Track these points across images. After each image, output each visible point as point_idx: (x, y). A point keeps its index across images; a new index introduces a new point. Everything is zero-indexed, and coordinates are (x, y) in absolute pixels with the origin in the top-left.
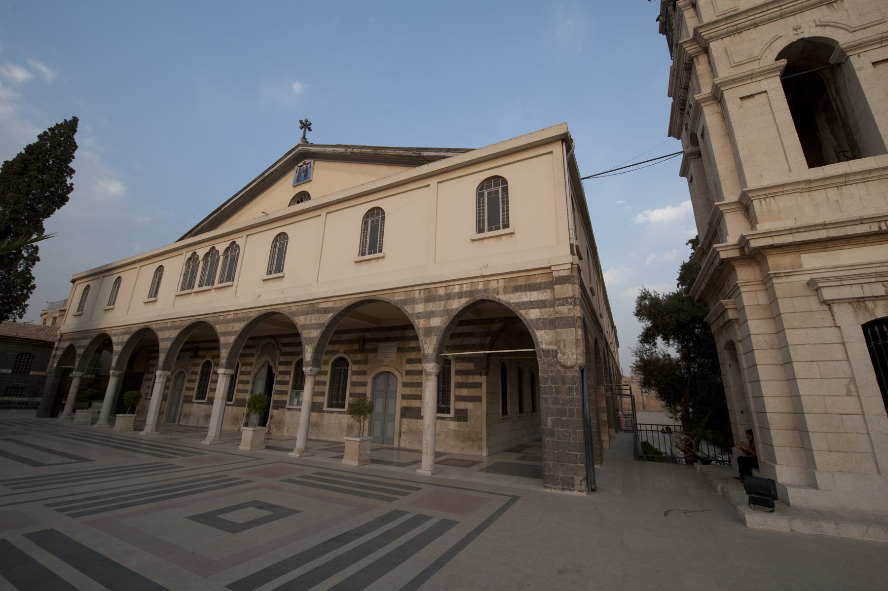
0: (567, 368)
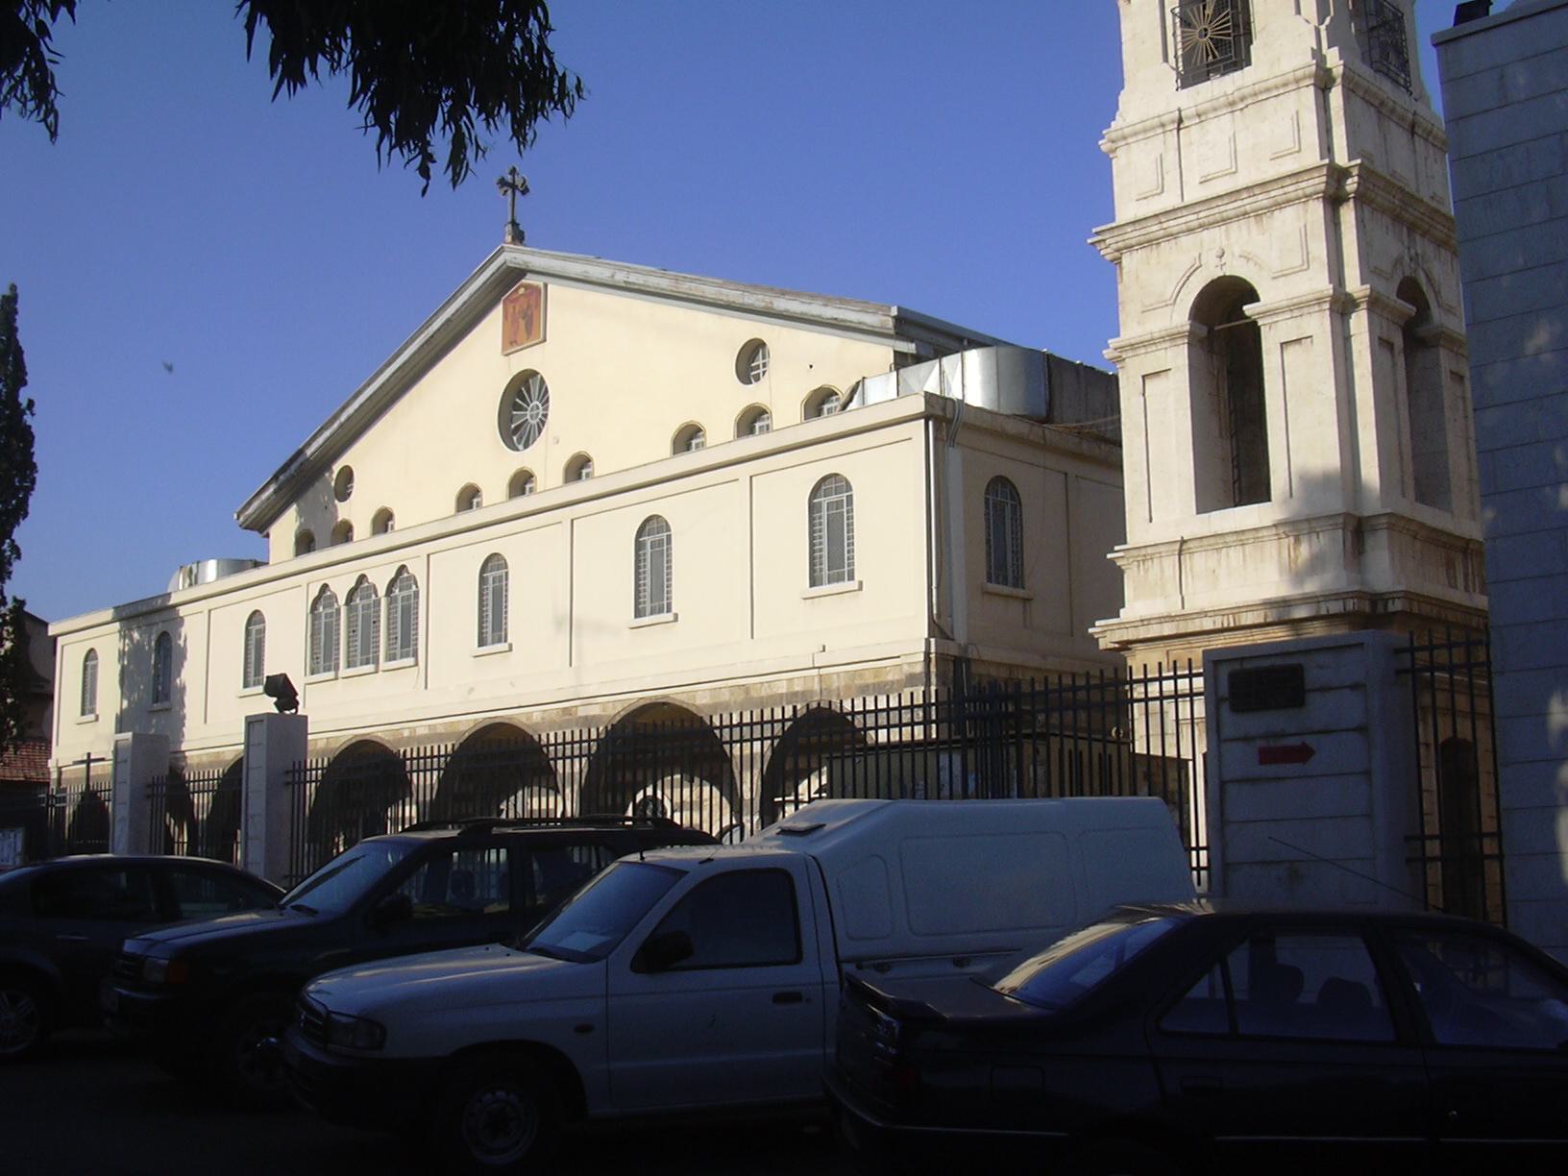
0: (1064, 835)
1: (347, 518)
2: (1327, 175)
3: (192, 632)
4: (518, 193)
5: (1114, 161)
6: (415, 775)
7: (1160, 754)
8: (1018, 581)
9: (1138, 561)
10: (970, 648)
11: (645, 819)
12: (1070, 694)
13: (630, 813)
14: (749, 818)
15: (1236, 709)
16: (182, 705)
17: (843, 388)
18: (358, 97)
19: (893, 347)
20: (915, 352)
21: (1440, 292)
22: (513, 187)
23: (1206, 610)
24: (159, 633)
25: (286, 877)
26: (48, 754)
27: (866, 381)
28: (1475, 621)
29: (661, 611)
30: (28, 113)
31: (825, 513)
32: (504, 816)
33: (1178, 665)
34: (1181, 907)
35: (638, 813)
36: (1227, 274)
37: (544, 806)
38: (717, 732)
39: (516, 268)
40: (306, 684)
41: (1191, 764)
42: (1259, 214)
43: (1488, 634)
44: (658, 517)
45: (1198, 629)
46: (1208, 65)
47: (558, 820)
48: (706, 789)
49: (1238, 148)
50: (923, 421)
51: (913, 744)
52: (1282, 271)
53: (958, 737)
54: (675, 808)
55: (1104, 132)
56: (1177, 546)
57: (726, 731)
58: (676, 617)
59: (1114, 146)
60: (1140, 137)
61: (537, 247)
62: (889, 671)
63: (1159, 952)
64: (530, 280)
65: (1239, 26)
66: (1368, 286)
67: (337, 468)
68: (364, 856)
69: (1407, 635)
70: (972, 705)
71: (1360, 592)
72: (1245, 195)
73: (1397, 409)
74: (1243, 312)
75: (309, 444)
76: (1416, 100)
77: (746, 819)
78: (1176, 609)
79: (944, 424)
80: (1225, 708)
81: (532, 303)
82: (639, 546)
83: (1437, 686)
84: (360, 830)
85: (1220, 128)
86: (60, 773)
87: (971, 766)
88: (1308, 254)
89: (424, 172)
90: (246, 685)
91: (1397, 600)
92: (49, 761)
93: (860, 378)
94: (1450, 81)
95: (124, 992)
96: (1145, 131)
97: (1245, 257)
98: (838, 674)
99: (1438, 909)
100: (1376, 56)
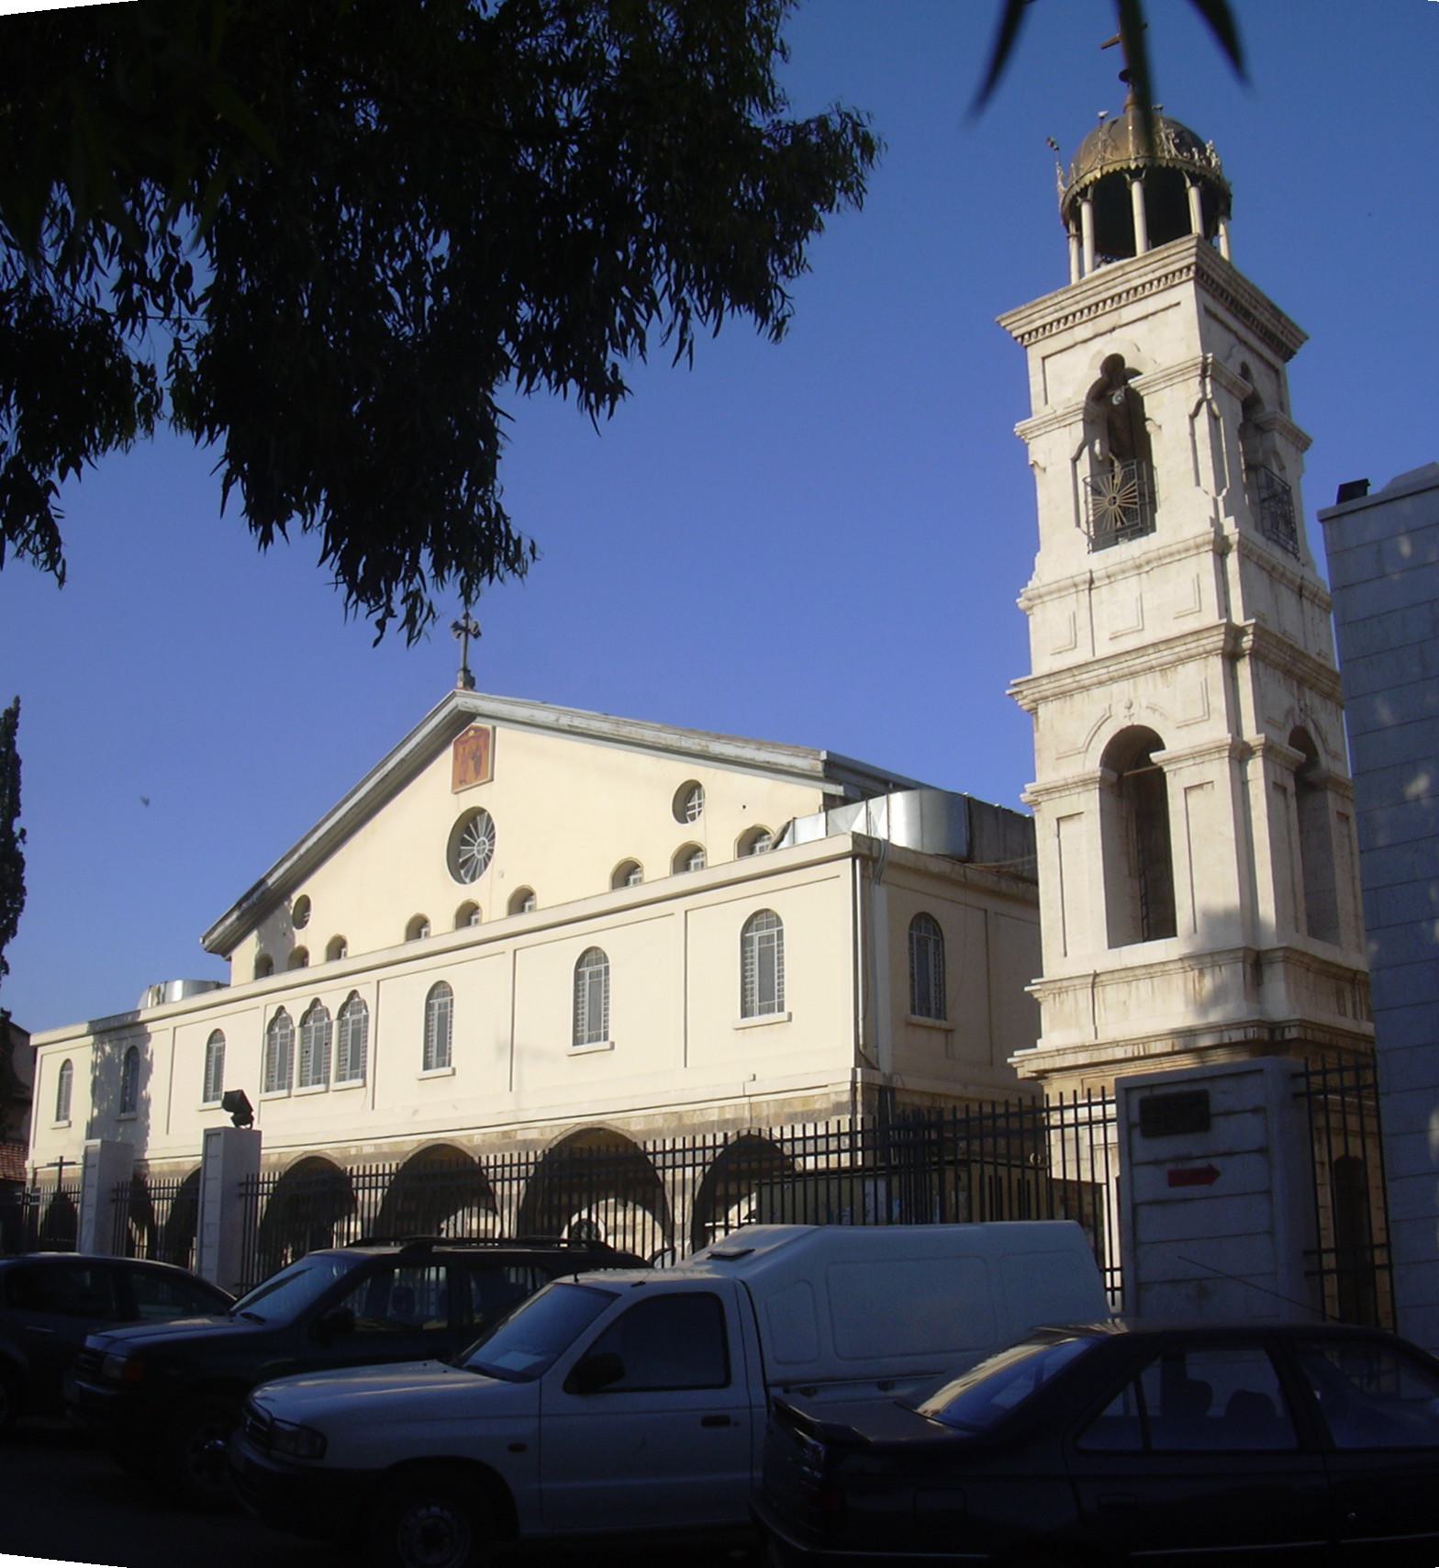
1: (303, 944)
2: (1226, 634)
3: (158, 1047)
4: (471, 637)
5: (1031, 618)
6: (360, 1192)
7: (1075, 1178)
8: (941, 1014)
10: (895, 1077)
11: (579, 1241)
12: (990, 1122)
13: (565, 1235)
14: (680, 1242)
15: (1146, 1134)
16: (147, 1116)
17: (775, 828)
18: (329, 554)
20: (842, 794)
22: (466, 630)
24: (129, 1046)
25: (237, 1285)
26: (24, 1153)
27: (797, 821)
28: (1362, 1047)
29: (598, 1039)
30: (41, 563)
31: (756, 947)
32: (444, 1235)
33: (1092, 1092)
34: (1097, 1327)
35: (573, 1235)
36: (1135, 724)
37: (482, 1227)
38: (650, 1158)
41: (1104, 1187)
42: (1164, 668)
43: (1375, 1060)
45: (1110, 1058)
46: (1117, 531)
47: (496, 1241)
48: (639, 1214)
49: (1145, 608)
50: (850, 860)
51: (840, 1171)
53: (883, 1164)
54: (609, 1231)
55: (1022, 591)
56: (1091, 979)
57: (659, 1157)
58: (613, 1045)
59: (1030, 604)
60: (1055, 596)
61: (486, 692)
63: (1076, 1371)
64: (479, 723)
67: (295, 897)
68: (310, 1269)
69: (1303, 1061)
70: (897, 1133)
71: (1259, 1021)
72: (1151, 651)
74: (1150, 759)
75: (270, 874)
76: (1303, 565)
77: (678, 1243)
78: (1090, 1039)
79: (870, 863)
80: (1136, 1133)
82: (578, 977)
83: (1330, 1107)
84: (308, 1243)
85: (1128, 589)
86: (35, 1174)
87: (895, 1192)
89: (381, 625)
90: (206, 1100)
91: (1293, 1029)
92: (27, 1162)
93: (791, 819)
95: (84, 1385)
96: (1059, 591)
97: (1151, 708)
98: (768, 1102)
99: (1335, 1319)
100: (1267, 524)
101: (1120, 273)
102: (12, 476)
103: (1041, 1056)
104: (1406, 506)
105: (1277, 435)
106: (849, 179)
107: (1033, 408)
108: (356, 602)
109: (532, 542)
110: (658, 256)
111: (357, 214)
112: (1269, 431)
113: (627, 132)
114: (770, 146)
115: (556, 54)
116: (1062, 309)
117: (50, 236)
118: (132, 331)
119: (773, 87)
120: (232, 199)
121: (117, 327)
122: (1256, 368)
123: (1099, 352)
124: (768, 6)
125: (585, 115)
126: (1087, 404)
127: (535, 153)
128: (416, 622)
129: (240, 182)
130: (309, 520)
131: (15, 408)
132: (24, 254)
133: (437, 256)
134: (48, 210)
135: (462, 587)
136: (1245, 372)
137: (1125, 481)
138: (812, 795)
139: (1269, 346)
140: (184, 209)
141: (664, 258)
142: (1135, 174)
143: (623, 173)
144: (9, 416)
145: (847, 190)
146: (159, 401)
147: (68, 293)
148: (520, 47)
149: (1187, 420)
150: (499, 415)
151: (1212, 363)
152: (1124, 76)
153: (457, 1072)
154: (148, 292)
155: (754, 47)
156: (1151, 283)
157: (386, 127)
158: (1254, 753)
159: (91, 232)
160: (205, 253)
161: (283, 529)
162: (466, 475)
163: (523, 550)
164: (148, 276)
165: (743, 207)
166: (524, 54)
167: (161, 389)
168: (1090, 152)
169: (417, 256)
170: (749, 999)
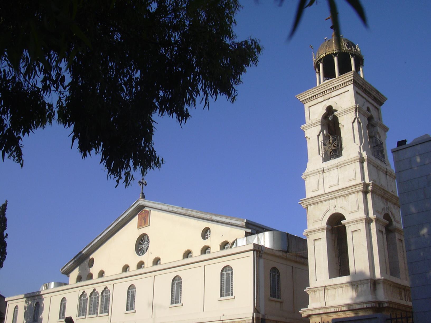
2: (364, 186)
3: (46, 302)
4: (144, 185)
5: (306, 181)
8: (279, 297)
9: (313, 292)
17: (231, 242)
19: (245, 230)
20: (251, 232)
21: (395, 217)
22: (143, 183)
23: (332, 306)
24: (37, 302)
27: (237, 240)
28: (408, 309)
29: (178, 303)
30: (16, 160)
31: (225, 276)
36: (337, 212)
39: (142, 205)
40: (77, 319)
42: (345, 196)
44: (178, 276)
45: (330, 311)
46: (331, 156)
49: (339, 178)
50: (253, 251)
52: (352, 211)
55: (303, 173)
56: (324, 288)
58: (182, 304)
59: (306, 177)
62: (242, 322)
64: (146, 209)
65: (339, 146)
66: (375, 216)
72: (341, 191)
73: (384, 249)
74: (341, 223)
76: (387, 165)
78: (324, 306)
79: (259, 252)
81: (146, 215)
82: (173, 284)
85: (334, 173)
88: (359, 207)
89: (118, 181)
90: (60, 318)
91: (386, 304)
93: (236, 239)
94: (396, 162)
96: (314, 173)
97: (342, 208)
100: (376, 153)
101: (331, 82)
102: (8, 134)
103: (309, 310)
104: (418, 147)
105: (378, 128)
106: (253, 58)
107: (306, 121)
108: (111, 174)
109: (162, 158)
110: (199, 79)
111: (114, 64)
112: (376, 126)
113: (191, 44)
114: (231, 48)
115: (171, 22)
116: (314, 93)
117: (23, 65)
118: (46, 94)
119: (232, 33)
120: (77, 58)
121: (42, 92)
122: (371, 108)
123: (325, 105)
124: (231, 11)
125: (179, 39)
126: (322, 120)
127: (165, 49)
128: (128, 181)
129: (80, 53)
130: (97, 151)
131: (10, 114)
132: (14, 69)
133: (136, 77)
134: (22, 57)
135: (142, 171)
136: (368, 109)
137: (333, 142)
138: (242, 232)
139: (375, 102)
140: (63, 60)
141: (201, 79)
142: (335, 55)
143: (190, 56)
144: (8, 116)
145: (253, 61)
146: (54, 115)
147: (27, 82)
148: (161, 20)
149: (351, 123)
150: (153, 122)
151: (358, 107)
152: (332, 28)
153: (136, 312)
154: (52, 83)
155: (227, 22)
156: (340, 85)
157: (123, 41)
158: (373, 221)
159: (35, 65)
160: (69, 73)
161: (90, 153)
162: (143, 139)
163: (159, 161)
164: (52, 78)
165: (224, 65)
166: (162, 22)
167: (55, 111)
168: (322, 49)
169: (131, 77)
170: (223, 292)
